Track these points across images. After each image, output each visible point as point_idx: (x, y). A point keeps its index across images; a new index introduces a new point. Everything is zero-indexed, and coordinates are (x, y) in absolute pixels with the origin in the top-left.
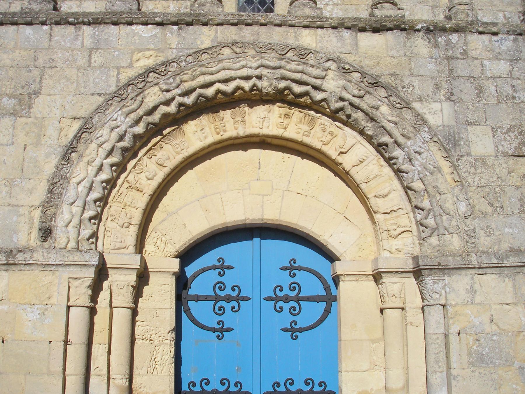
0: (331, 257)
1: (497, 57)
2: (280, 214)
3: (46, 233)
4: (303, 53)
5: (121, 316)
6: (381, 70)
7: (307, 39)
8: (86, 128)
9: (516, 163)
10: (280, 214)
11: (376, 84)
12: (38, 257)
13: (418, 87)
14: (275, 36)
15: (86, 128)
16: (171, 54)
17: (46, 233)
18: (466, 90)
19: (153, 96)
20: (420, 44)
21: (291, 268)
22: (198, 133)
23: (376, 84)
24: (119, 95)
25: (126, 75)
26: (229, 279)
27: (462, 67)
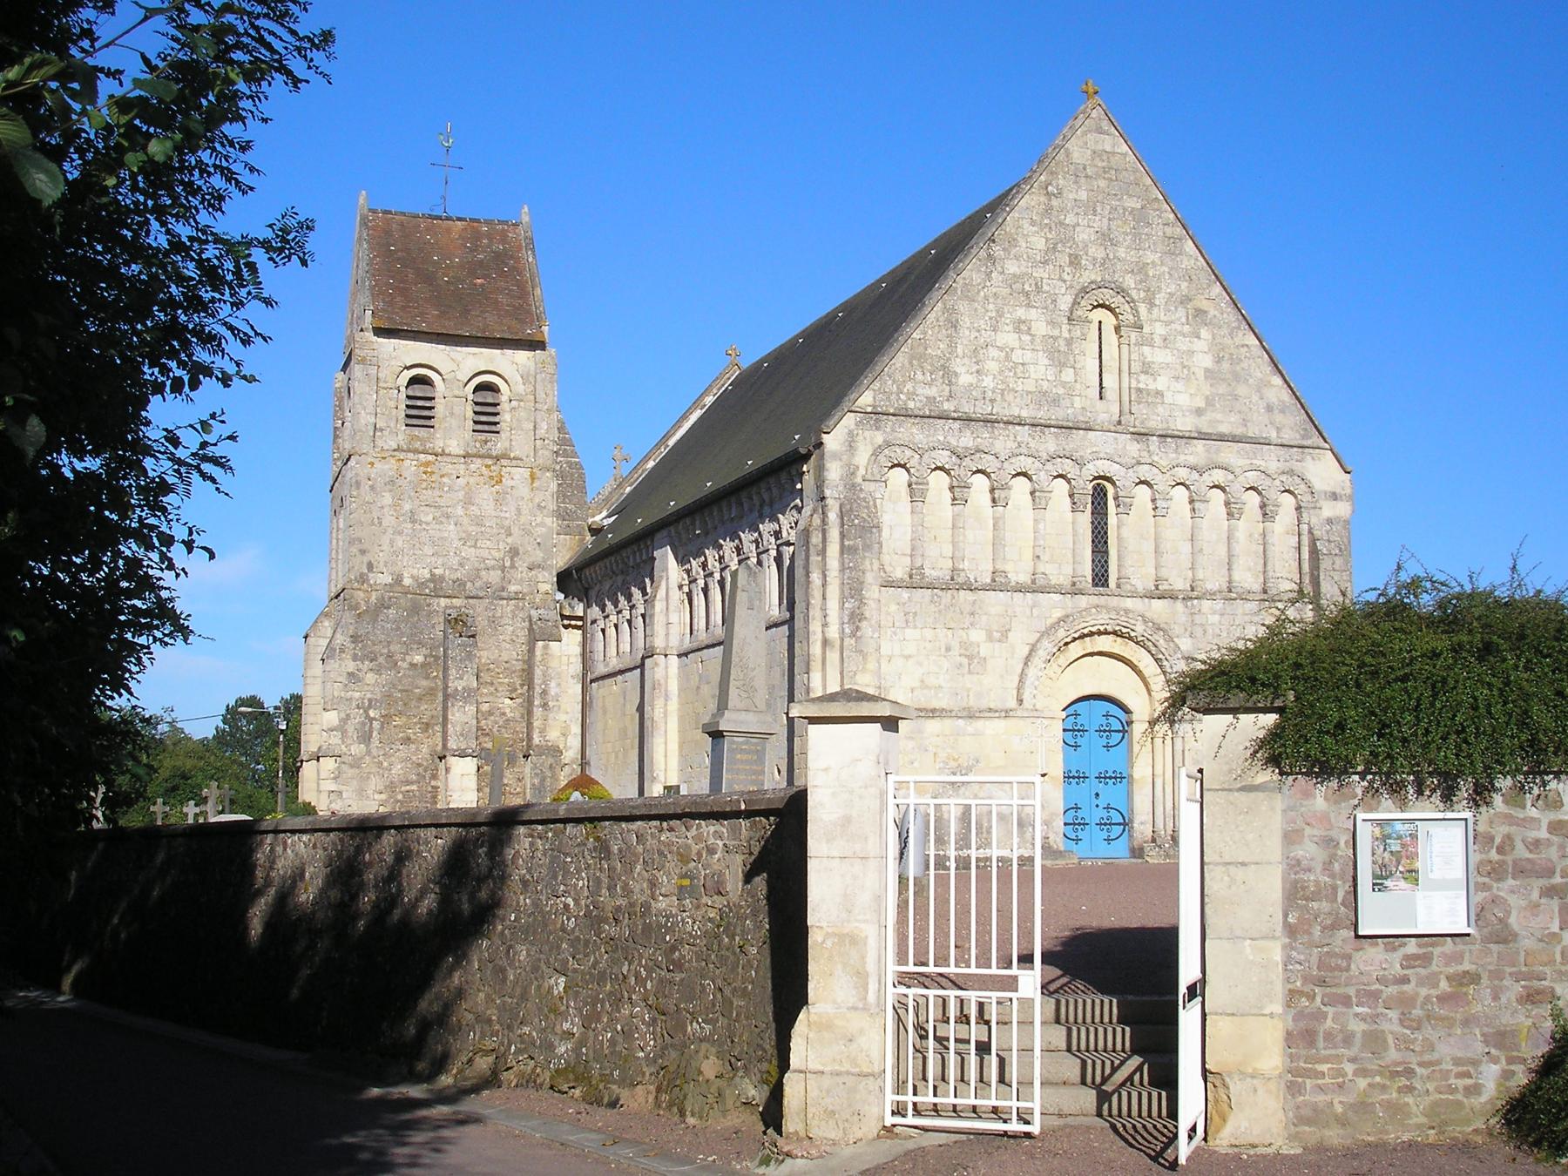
0: (1127, 711)
1: (1214, 613)
2: (276, 832)
3: (1020, 702)
4: (1127, 611)
5: (1159, 771)
6: (1160, 621)
7: (1129, 603)
8: (1033, 649)
9: (654, 779)
10: (276, 832)
11: (1159, 629)
12: (1019, 713)
13: (1177, 630)
14: (1114, 602)
15: (1033, 649)
16: (1069, 611)
17: (1020, 702)
18: (1198, 631)
19: (1061, 633)
20: (1179, 605)
21: (1107, 716)
22: (1105, 643)
23: (1159, 629)
24: (1046, 633)
25: (1050, 621)
26: (1080, 720)
27: (1198, 619)
